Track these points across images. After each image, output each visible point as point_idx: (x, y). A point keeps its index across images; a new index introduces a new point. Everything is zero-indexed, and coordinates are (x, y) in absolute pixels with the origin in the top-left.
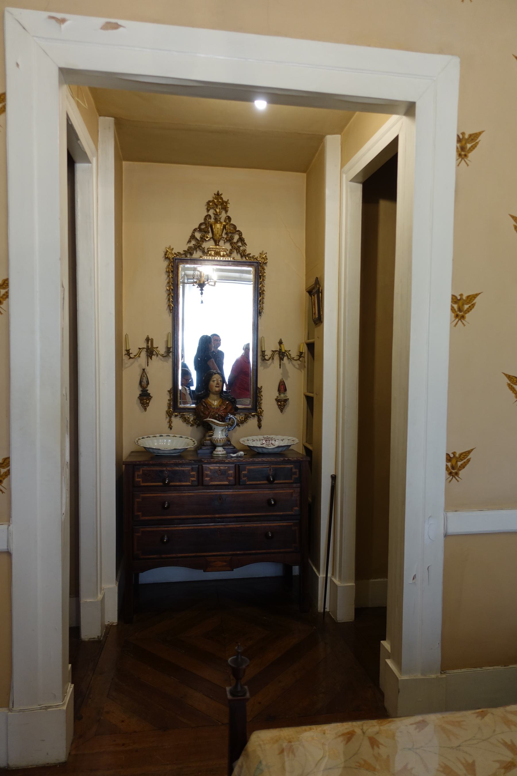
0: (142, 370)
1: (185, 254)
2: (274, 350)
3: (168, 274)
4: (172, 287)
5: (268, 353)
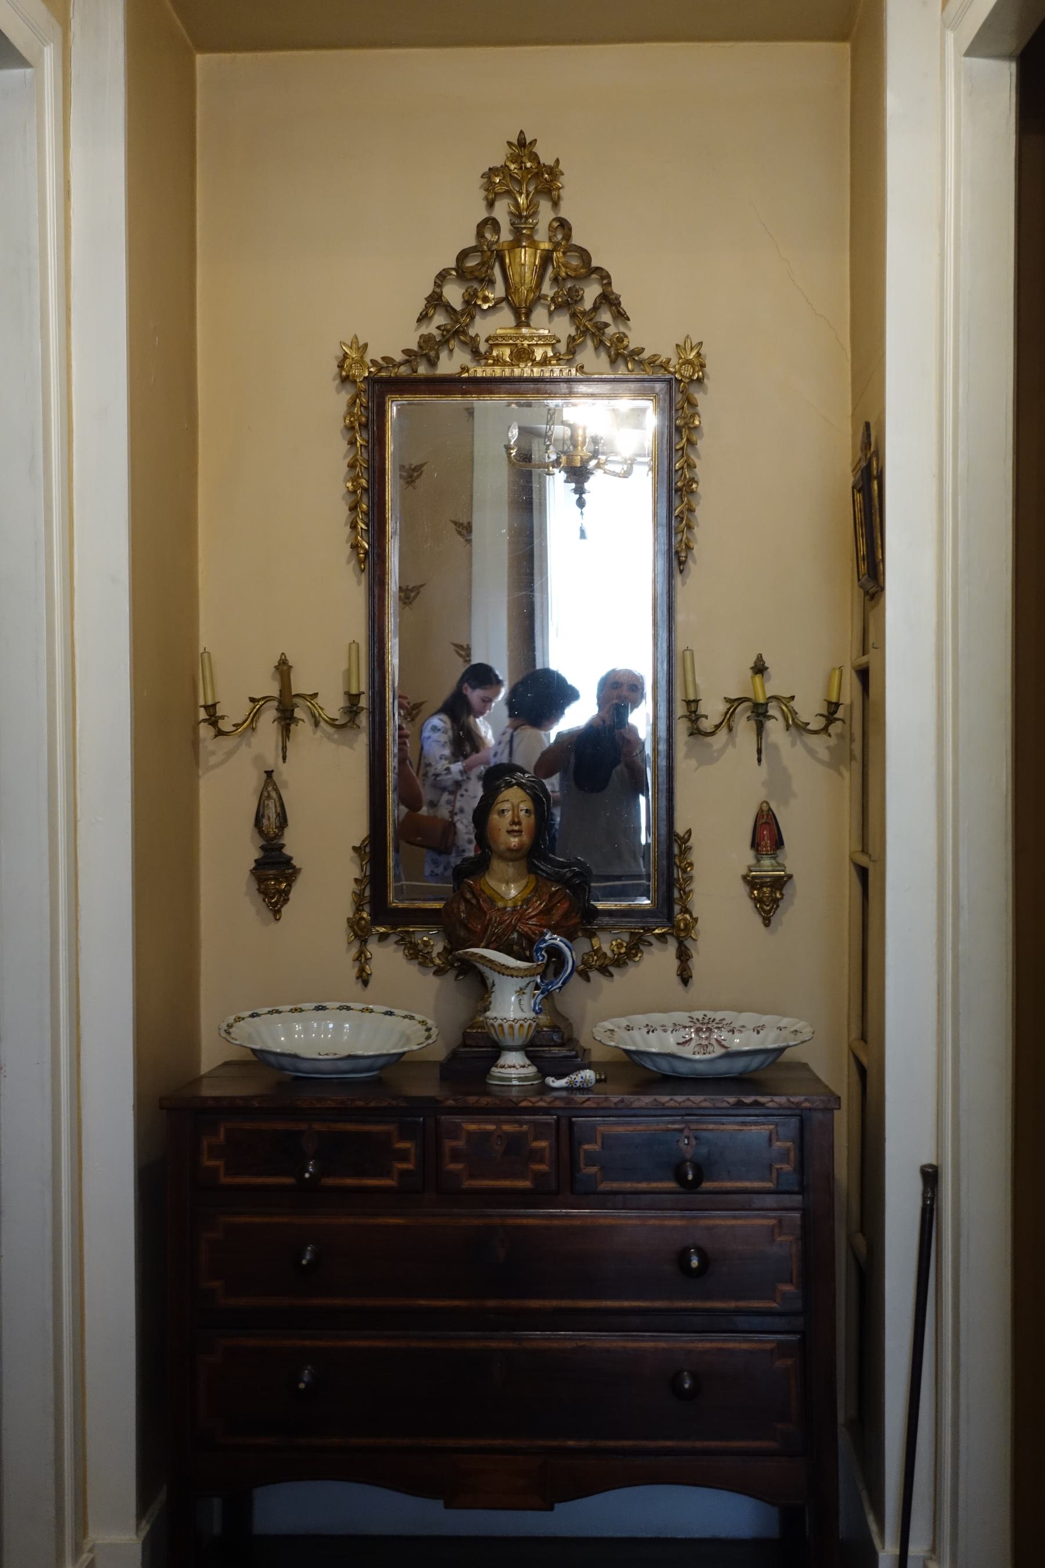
0: (264, 776)
1: (407, 362)
2: (733, 697)
3: (349, 435)
4: (364, 482)
5: (712, 710)
